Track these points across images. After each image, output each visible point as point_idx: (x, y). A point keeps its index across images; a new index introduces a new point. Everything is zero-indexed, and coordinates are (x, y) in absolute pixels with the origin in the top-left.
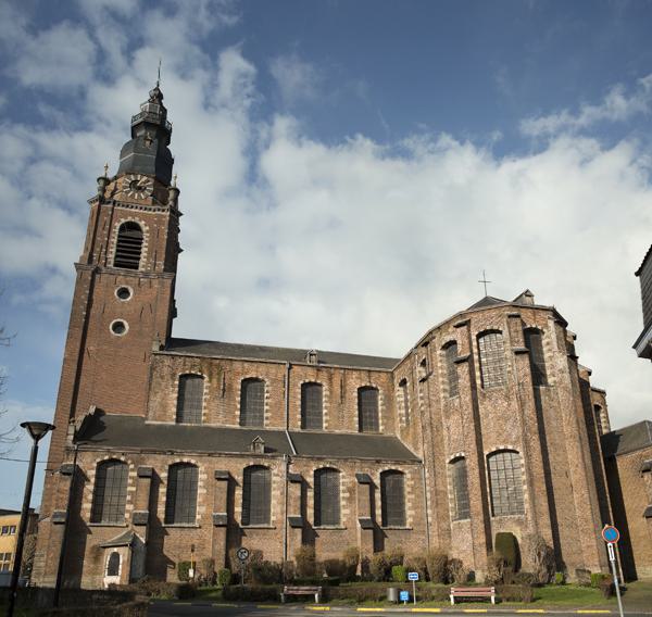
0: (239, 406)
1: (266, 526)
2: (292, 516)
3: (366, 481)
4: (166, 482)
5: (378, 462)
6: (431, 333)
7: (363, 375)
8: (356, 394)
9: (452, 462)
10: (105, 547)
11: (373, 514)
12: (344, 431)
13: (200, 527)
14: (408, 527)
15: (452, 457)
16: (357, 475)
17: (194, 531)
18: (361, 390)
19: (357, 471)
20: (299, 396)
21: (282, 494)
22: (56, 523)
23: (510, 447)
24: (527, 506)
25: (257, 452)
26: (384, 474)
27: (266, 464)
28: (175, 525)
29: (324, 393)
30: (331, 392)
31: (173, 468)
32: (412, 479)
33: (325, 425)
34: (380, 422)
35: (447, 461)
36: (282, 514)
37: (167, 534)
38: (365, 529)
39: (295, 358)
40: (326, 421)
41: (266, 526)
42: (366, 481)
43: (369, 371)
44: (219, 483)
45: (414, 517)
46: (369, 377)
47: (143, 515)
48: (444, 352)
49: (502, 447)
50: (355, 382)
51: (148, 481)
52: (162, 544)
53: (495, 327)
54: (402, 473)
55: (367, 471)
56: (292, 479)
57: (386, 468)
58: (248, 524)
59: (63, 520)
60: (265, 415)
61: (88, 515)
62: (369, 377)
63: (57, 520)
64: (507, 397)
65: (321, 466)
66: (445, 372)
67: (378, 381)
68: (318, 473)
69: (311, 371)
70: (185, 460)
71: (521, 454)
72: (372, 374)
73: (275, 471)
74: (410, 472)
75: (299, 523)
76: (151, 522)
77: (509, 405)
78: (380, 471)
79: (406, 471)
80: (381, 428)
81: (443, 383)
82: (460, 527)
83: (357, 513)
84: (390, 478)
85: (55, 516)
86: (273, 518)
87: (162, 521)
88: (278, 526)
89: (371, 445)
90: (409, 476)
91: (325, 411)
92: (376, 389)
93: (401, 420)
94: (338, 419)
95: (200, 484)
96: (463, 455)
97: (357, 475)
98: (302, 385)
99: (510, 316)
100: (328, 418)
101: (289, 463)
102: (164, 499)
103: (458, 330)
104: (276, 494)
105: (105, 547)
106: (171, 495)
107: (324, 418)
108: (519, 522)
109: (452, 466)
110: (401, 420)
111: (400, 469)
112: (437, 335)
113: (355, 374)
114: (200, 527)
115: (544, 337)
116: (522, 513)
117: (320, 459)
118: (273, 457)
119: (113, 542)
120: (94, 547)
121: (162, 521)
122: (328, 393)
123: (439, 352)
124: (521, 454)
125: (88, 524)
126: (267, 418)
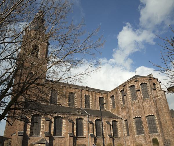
0: (68, 100)
1: (82, 137)
2: (91, 133)
3: (91, 123)
4: (54, 122)
5: (111, 118)
6: (125, 83)
7: (100, 94)
8: (99, 99)
9: (134, 118)
10: (35, 144)
11: (73, 132)
12: (96, 109)
13: (64, 137)
14: (119, 137)
15: (135, 117)
16: (106, 122)
17: (62, 139)
18: (100, 98)
19: (106, 120)
20: (84, 99)
21: (87, 127)
22: (19, 136)
23: (153, 115)
24: (159, 131)
25: (79, 114)
26: (113, 122)
27: (82, 118)
28: (56, 136)
29: (90, 98)
30: (92, 98)
31: (77, 119)
32: (120, 123)
33: (91, 107)
34: (105, 107)
35: (133, 118)
36: (87, 133)
37: (54, 140)
38: (92, 137)
39: (82, 88)
40: (92, 106)
41: (82, 137)
42: (109, 123)
43: (102, 93)
44: (70, 123)
45: (121, 134)
46: (102, 95)
47: (48, 133)
48: (129, 88)
49: (150, 114)
50: (98, 96)
51: (49, 122)
52: (53, 143)
53: (145, 82)
54: (117, 121)
55: (108, 120)
56: (91, 123)
57: (113, 120)
58: (55, 136)
59: (22, 135)
60: (75, 103)
61: (29, 133)
62: (102, 95)
63: (20, 134)
64: (150, 101)
65: (97, 119)
66: (130, 94)
67: (104, 96)
68: (96, 120)
69: (87, 92)
70: (59, 116)
71: (156, 116)
72: (102, 94)
73: (85, 120)
74: (119, 121)
75: (92, 136)
76: (49, 135)
77: (151, 103)
78: (112, 121)
79: (118, 121)
80: (105, 109)
81: (130, 96)
82: (139, 137)
83: (107, 133)
84: (114, 122)
85: (19, 133)
86: (85, 134)
87: (53, 135)
88: (86, 137)
89: (102, 113)
90: (119, 122)
91: (91, 103)
92: (103, 98)
93: (111, 107)
94: (95, 106)
95: (63, 123)
96: (141, 117)
97: (106, 122)
98: (85, 96)
99: (150, 80)
100: (92, 105)
101: (89, 118)
102: (53, 128)
103: (136, 82)
104: (85, 127)
105: (35, 144)
106: (55, 127)
107: (91, 105)
108: (157, 136)
109: (134, 119)
110: (111, 107)
111: (116, 120)
112: (127, 84)
113: (98, 94)
114: (64, 137)
115: (156, 86)
116: (157, 133)
117: (96, 117)
118: (84, 116)
119: (38, 142)
120: (31, 144)
121: (53, 135)
122: (92, 98)
123: (128, 88)
124: (156, 116)
125: (29, 136)
126: (76, 104)
